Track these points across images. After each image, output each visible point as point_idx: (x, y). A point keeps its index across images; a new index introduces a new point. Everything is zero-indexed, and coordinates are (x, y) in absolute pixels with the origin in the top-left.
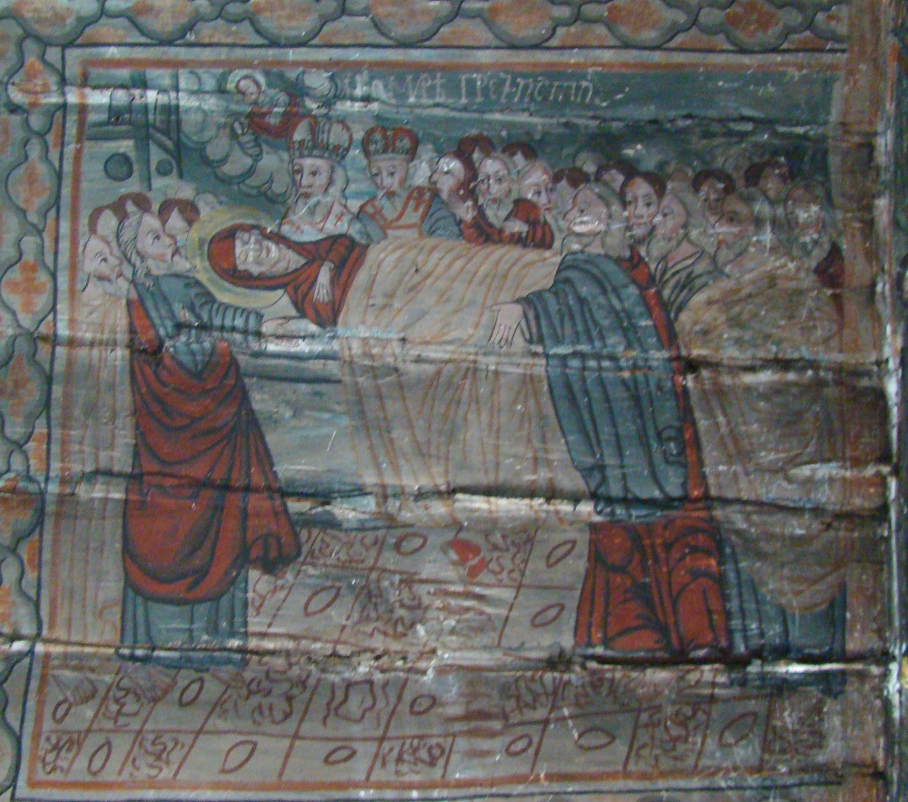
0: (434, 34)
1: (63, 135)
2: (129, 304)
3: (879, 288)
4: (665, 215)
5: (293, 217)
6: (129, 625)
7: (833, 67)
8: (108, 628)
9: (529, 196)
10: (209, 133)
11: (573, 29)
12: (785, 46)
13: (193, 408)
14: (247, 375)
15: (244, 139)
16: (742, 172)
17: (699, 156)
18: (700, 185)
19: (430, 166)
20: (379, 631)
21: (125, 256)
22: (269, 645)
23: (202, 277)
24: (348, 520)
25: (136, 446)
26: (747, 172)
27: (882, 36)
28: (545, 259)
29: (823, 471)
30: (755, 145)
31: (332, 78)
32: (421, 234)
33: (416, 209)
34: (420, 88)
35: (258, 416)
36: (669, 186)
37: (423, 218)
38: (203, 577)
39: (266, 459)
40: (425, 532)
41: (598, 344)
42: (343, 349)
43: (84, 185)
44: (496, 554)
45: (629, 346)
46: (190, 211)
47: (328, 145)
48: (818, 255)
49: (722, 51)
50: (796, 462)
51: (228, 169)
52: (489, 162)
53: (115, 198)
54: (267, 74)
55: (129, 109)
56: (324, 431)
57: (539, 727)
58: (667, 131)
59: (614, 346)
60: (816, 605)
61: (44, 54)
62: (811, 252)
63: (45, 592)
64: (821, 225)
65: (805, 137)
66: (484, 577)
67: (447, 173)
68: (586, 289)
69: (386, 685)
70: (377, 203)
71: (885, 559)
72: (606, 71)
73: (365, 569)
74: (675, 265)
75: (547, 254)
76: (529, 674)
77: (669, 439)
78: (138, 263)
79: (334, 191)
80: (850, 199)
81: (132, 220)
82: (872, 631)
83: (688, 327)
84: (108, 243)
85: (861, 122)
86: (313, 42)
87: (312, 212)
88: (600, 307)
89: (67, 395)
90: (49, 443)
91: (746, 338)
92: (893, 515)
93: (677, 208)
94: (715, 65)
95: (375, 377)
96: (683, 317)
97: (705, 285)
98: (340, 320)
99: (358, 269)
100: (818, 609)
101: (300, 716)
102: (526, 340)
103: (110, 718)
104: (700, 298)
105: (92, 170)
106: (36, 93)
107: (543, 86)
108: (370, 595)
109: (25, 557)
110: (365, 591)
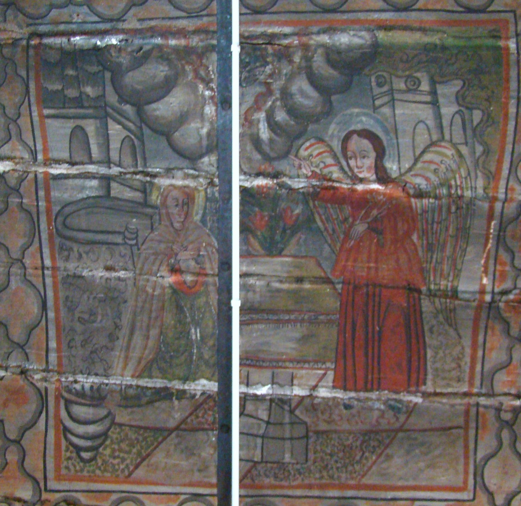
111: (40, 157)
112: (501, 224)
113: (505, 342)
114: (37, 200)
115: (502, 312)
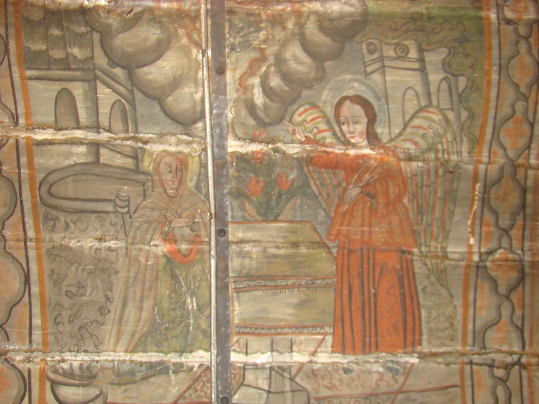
63: (527, 322)
90: (524, 230)
106: (520, 12)
109: (515, 301)
111: (22, 121)
112: (485, 186)
113: (495, 300)
114: (19, 167)
115: (489, 270)
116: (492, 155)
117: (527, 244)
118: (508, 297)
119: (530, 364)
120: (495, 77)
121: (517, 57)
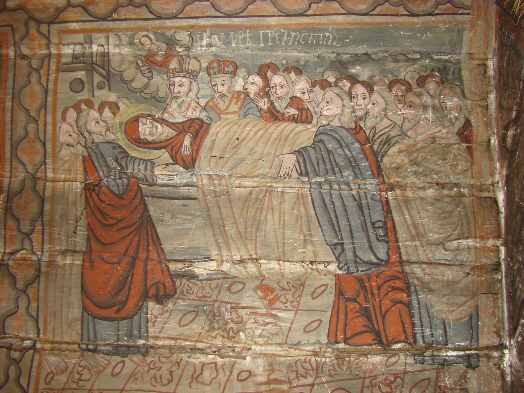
0: (245, 10)
1: (49, 70)
2: (83, 157)
3: (492, 142)
4: (373, 104)
5: (170, 110)
6: (85, 332)
7: (463, 23)
8: (74, 333)
9: (298, 95)
10: (124, 66)
11: (320, 5)
12: (436, 12)
13: (119, 214)
14: (146, 196)
15: (143, 68)
16: (415, 81)
17: (391, 72)
18: (393, 87)
19: (244, 80)
20: (220, 335)
21: (81, 133)
22: (160, 343)
23: (122, 143)
24: (202, 275)
25: (88, 235)
26: (417, 80)
27: (490, 5)
28: (308, 129)
29: (464, 243)
30: (422, 66)
31: (190, 35)
32: (239, 116)
33: (236, 104)
34: (238, 38)
35: (152, 218)
36: (375, 88)
37: (240, 108)
38: (124, 307)
39: (157, 241)
40: (244, 281)
41: (338, 175)
42: (198, 181)
43: (59, 96)
44: (284, 292)
45: (356, 176)
46: (115, 108)
47: (188, 70)
48: (459, 124)
49: (402, 15)
50: (448, 239)
51: (135, 85)
52: (276, 77)
53: (75, 102)
54: (155, 34)
55: (83, 55)
56: (189, 226)
57: (309, 388)
58: (374, 60)
59: (347, 177)
60: (462, 318)
61: (39, 28)
62: (454, 123)
63: (41, 314)
64: (460, 109)
65: (448, 61)
66: (278, 305)
67: (253, 83)
68: (331, 145)
69: (223, 365)
70: (215, 101)
71: (500, 292)
72: (339, 27)
73: (211, 301)
74: (380, 131)
75: (309, 126)
76: (303, 358)
77: (379, 227)
78: (87, 136)
79: (192, 95)
80: (475, 94)
81: (84, 114)
82: (494, 332)
83: (388, 166)
84: (71, 126)
85: (478, 54)
86: (179, 16)
87: (180, 106)
88: (339, 155)
89: (52, 209)
90: (43, 234)
91: (420, 171)
92: (503, 267)
93: (380, 100)
94: (398, 23)
95: (216, 196)
96: (386, 160)
97: (397, 142)
98: (197, 165)
99: (205, 137)
100: (463, 320)
101: (177, 381)
102: (299, 174)
103: (74, 382)
104: (394, 149)
105: (64, 88)
107: (305, 36)
108: (214, 316)
109: (30, 295)
110: (212, 313)
112: (8, 197)
113: (13, 294)
115: (10, 268)
116: (13, 170)
117: (47, 247)
118: (24, 291)
119: (43, 349)
120: (9, 104)
121: (28, 87)
